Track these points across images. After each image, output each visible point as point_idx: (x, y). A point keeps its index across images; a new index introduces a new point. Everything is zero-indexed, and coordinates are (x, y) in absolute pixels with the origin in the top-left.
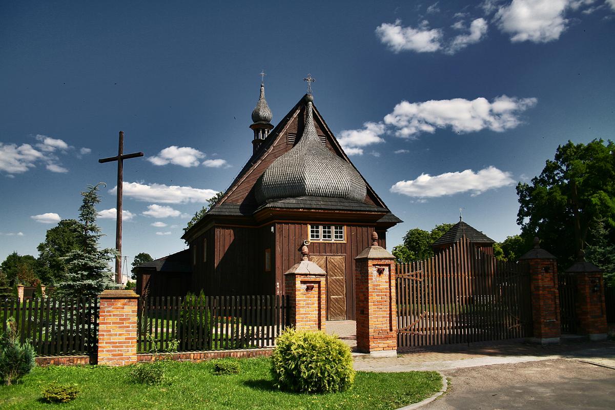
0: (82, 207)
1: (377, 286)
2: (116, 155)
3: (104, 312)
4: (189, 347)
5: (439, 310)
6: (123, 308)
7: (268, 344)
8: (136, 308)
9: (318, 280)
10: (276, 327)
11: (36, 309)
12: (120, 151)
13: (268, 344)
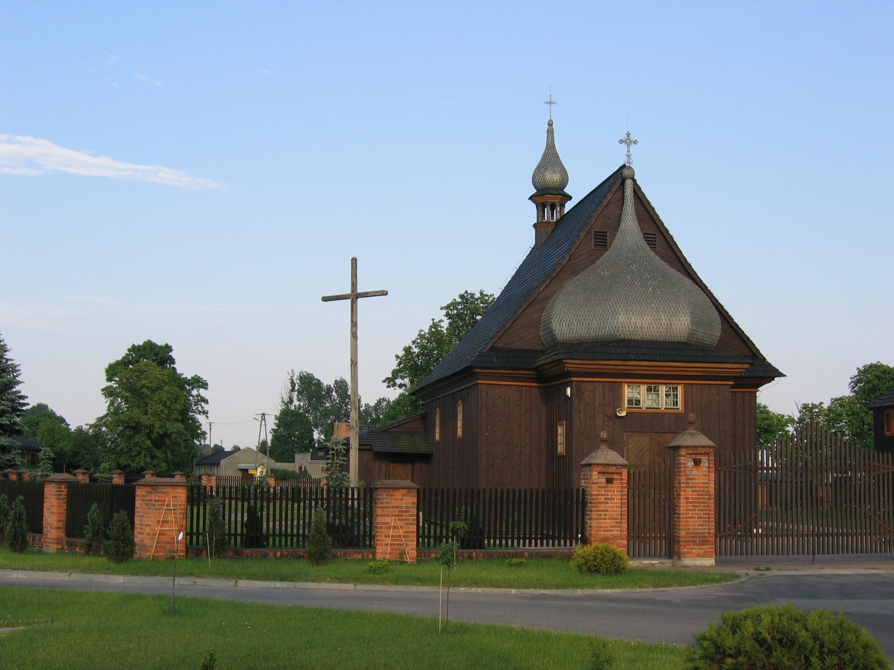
0: (387, 379)
1: (692, 479)
2: (348, 291)
3: (382, 503)
4: (471, 545)
5: (868, 526)
6: (402, 499)
7: (518, 544)
8: (415, 500)
9: (619, 471)
10: (202, 508)
11: (842, 535)
12: (354, 285)
13: (518, 544)
